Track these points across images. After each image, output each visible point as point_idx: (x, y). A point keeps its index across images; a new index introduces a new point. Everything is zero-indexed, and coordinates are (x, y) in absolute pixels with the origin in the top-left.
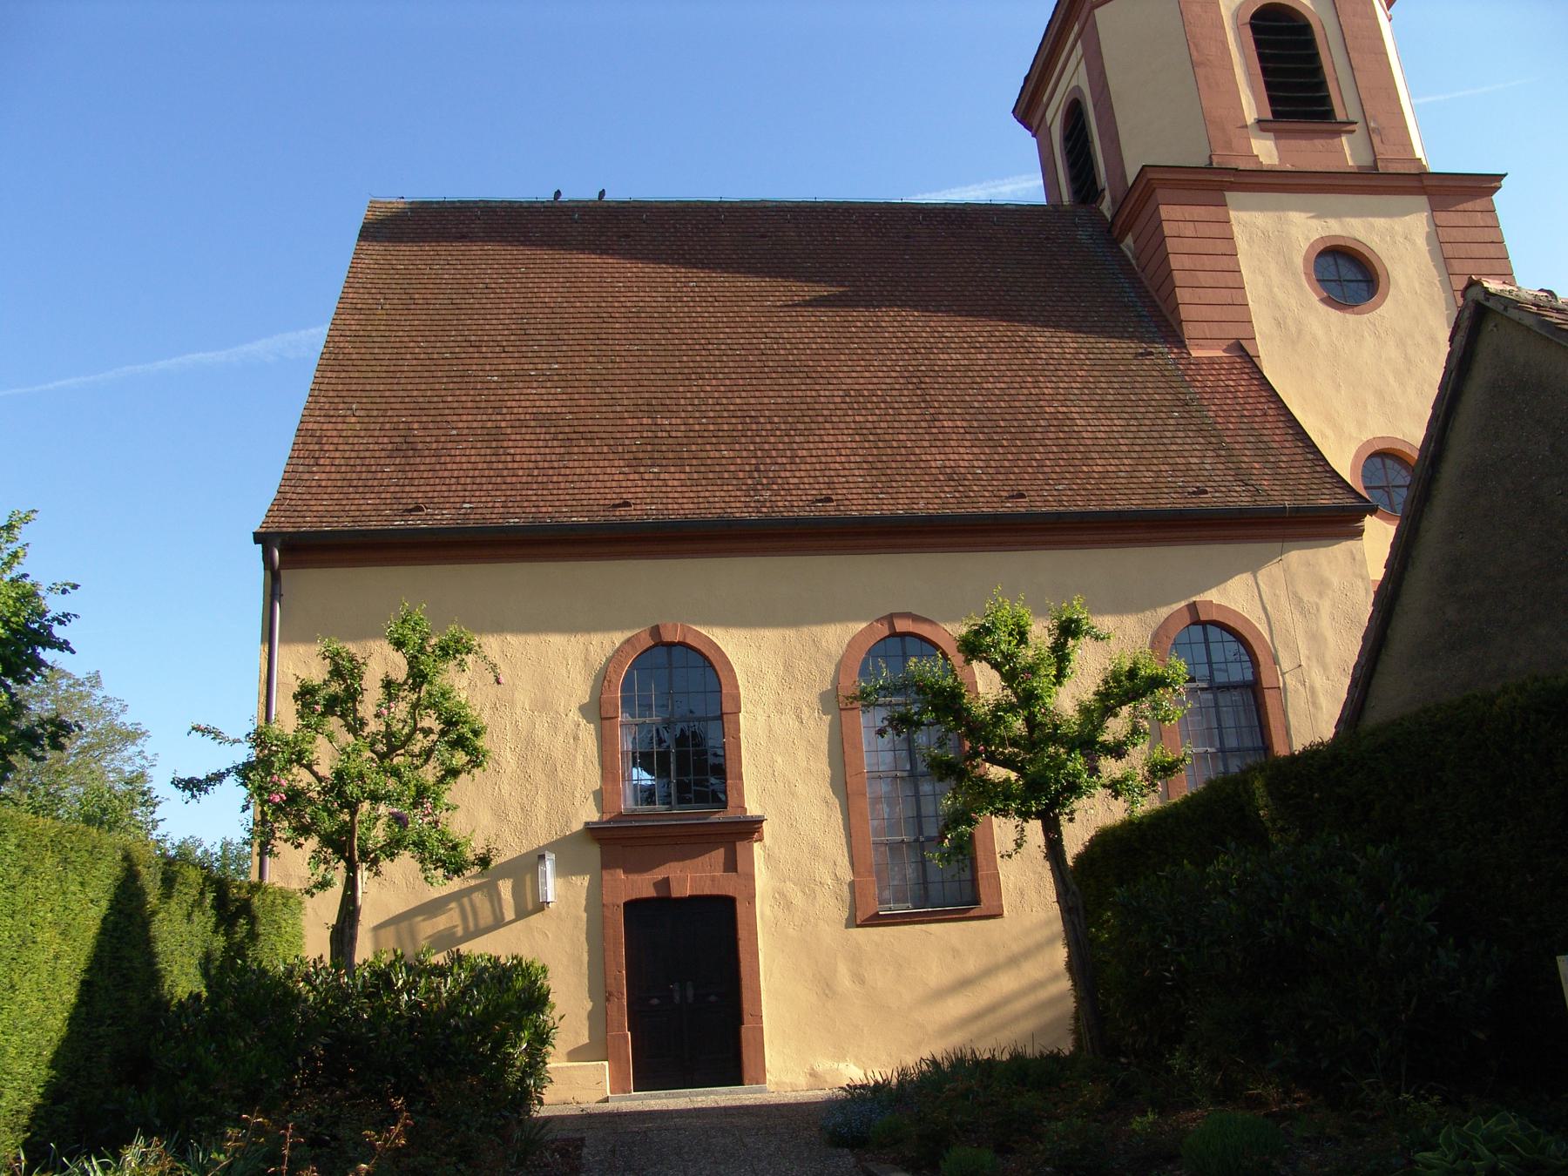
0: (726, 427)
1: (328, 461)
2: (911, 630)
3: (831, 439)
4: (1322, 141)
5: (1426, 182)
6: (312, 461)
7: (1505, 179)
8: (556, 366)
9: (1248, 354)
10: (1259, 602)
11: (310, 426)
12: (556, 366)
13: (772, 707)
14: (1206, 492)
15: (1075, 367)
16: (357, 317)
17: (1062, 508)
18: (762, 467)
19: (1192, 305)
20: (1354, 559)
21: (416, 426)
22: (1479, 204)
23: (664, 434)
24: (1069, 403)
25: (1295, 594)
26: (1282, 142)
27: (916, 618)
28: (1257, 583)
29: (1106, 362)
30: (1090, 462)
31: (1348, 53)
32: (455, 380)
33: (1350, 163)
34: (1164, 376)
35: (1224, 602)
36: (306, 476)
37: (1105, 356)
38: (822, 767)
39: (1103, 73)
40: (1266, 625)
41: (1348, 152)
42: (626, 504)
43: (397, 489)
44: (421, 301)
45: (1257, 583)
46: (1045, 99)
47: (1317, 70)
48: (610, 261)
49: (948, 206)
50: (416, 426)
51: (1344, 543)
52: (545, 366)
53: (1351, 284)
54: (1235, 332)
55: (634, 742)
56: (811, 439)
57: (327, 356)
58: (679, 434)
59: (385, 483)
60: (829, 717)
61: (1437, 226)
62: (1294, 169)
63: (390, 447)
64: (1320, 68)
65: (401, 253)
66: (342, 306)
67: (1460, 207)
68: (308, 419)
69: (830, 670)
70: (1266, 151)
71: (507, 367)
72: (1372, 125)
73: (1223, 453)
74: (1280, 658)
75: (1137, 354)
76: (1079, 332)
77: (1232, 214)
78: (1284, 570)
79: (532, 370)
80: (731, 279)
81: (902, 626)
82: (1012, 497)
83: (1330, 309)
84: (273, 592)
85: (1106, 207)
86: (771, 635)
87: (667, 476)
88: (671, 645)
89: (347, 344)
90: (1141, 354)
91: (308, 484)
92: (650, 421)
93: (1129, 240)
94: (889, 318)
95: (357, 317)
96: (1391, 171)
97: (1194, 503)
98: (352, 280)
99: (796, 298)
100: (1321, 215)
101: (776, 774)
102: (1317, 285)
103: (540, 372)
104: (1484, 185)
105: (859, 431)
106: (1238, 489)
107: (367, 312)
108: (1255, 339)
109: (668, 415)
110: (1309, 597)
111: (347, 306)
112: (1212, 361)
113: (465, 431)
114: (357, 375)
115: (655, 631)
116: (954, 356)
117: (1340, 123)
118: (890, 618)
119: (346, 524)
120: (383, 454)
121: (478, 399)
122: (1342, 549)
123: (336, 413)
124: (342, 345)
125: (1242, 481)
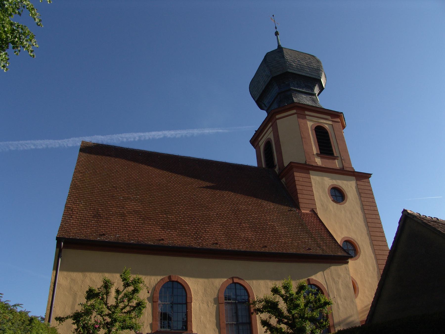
0: (186, 220)
1: (75, 217)
2: (238, 282)
3: (215, 226)
4: (331, 160)
5: (355, 174)
6: (70, 216)
7: (372, 175)
8: (138, 197)
9: (315, 213)
10: (324, 279)
11: (69, 205)
12: (138, 197)
13: (201, 301)
14: (311, 249)
15: (274, 212)
16: (80, 174)
17: (277, 251)
18: (198, 233)
19: (302, 198)
20: (346, 269)
21: (100, 209)
22: (366, 180)
23: (170, 220)
24: (274, 222)
25: (333, 278)
26: (322, 160)
27: (239, 279)
28: (324, 274)
29: (281, 212)
30: (281, 239)
31: (336, 140)
32: (110, 197)
33: (338, 167)
34: (296, 217)
35: (316, 279)
36: (69, 221)
37: (281, 210)
38: (214, 320)
39: (278, 136)
40: (326, 286)
41: (337, 164)
42: (163, 240)
43: (96, 228)
44: (98, 173)
45: (324, 274)
46: (259, 139)
47: (330, 143)
48: (150, 168)
49: (237, 165)
50: (100, 209)
51: (344, 265)
52: (135, 196)
53: (338, 197)
54: (312, 207)
55: (161, 309)
56: (209, 226)
57: (72, 185)
58: (174, 221)
59: (92, 225)
60: (216, 305)
61: (357, 184)
62: (325, 167)
63: (93, 215)
64: (330, 143)
65: (92, 157)
66: (76, 170)
67: (362, 181)
68: (68, 203)
69: (217, 292)
70: (318, 161)
71: (125, 195)
72: (342, 158)
73: (313, 239)
74: (330, 295)
75: (289, 210)
76: (274, 203)
77: (311, 176)
78: (330, 272)
79: (132, 197)
80: (184, 178)
81: (236, 280)
82: (264, 247)
83: (334, 203)
84: (58, 255)
85: (277, 169)
86: (201, 280)
87: (172, 233)
88: (173, 281)
89: (78, 182)
90: (290, 210)
91: (69, 223)
92: (166, 216)
93: (284, 179)
94: (225, 193)
95: (80, 174)
96: (347, 170)
97: (308, 252)
98: (78, 163)
99: (201, 185)
100: (332, 179)
101: (201, 321)
102: (331, 196)
103: (134, 198)
104: (367, 176)
105: (222, 225)
106: (318, 249)
107: (83, 173)
108: (316, 209)
109: (171, 215)
110: (336, 279)
111: (77, 171)
112: (307, 214)
113: (114, 213)
114: (81, 192)
115: (170, 277)
116: (244, 206)
117: (335, 156)
118: (232, 278)
119: (83, 237)
120: (91, 217)
121: (117, 204)
122: (344, 266)
123: (76, 202)
124: (77, 182)
125: (319, 247)
